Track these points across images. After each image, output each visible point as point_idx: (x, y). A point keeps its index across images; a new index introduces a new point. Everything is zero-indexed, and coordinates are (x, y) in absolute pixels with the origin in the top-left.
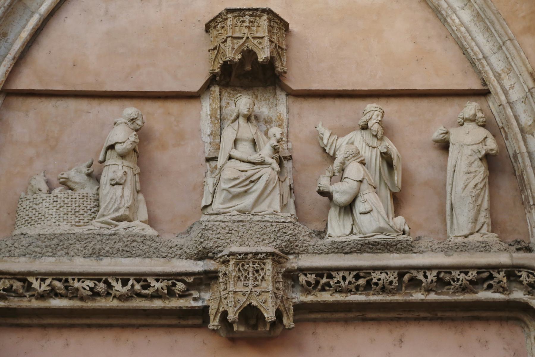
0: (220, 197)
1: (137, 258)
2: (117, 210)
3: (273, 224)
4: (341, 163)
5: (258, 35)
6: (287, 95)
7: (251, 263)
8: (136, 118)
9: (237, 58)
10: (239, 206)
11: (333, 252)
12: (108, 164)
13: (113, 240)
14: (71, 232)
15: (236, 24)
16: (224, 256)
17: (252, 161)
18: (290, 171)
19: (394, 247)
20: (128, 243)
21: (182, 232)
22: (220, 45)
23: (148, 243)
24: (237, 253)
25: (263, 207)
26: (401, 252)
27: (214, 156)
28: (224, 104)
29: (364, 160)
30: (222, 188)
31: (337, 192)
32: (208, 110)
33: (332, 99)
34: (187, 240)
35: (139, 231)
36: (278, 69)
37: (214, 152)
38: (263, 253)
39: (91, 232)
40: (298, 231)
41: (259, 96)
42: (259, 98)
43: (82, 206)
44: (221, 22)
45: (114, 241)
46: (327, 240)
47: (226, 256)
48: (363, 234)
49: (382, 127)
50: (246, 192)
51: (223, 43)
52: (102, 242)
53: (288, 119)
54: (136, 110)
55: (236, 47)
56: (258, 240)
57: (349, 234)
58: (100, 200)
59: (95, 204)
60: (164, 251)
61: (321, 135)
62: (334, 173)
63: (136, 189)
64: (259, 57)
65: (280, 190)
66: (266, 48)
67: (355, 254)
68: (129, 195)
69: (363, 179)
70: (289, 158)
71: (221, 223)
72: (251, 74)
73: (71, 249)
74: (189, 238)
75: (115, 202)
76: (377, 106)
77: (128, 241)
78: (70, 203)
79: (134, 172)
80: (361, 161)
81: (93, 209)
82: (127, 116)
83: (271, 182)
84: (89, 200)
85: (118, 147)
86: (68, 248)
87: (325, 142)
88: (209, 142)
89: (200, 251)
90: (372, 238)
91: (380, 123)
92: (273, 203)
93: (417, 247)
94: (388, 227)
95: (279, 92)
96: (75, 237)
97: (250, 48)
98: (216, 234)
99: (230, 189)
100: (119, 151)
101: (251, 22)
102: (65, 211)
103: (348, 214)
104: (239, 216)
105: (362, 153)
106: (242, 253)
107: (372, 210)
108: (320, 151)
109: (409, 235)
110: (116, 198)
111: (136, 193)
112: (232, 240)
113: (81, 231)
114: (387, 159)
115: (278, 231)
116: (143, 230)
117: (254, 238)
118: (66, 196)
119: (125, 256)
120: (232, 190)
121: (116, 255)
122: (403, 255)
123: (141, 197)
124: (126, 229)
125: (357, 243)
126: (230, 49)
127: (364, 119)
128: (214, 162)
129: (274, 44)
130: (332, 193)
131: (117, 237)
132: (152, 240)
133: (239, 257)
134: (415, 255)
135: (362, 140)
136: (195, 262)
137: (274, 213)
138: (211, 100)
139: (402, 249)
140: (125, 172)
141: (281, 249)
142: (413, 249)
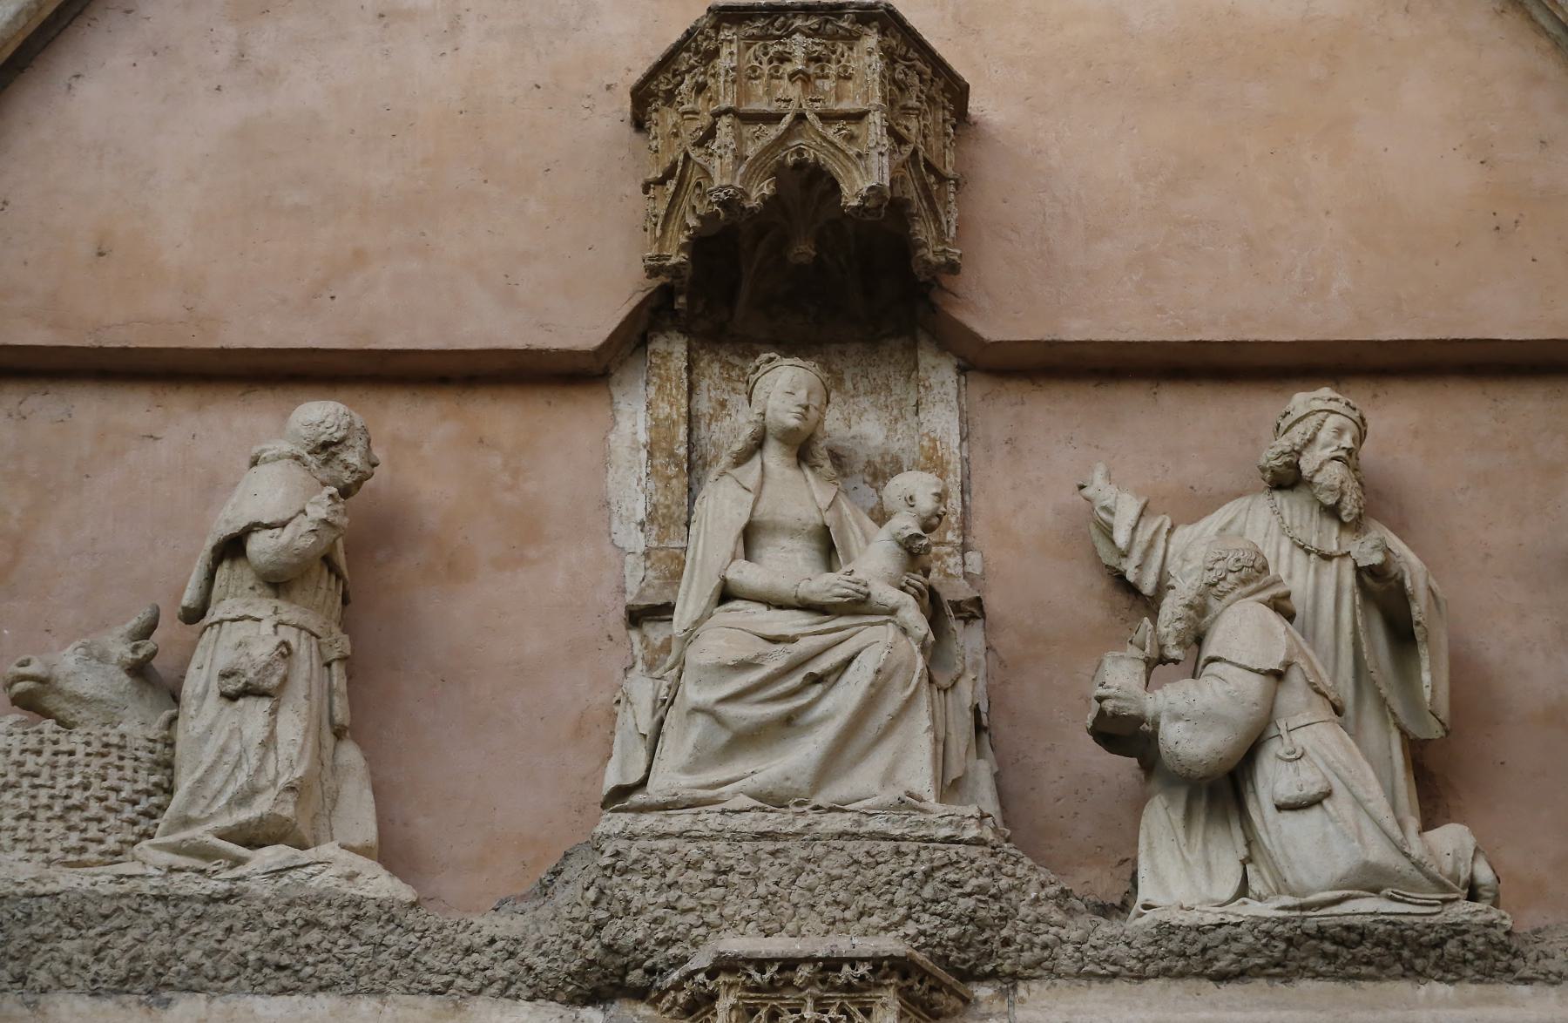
0: (675, 750)
1: (320, 996)
2: (244, 798)
3: (904, 846)
4: (1190, 606)
5: (846, 106)
6: (962, 370)
7: (810, 1003)
8: (341, 441)
9: (754, 194)
10: (758, 778)
11: (1165, 973)
12: (215, 619)
13: (218, 919)
14: (40, 889)
15: (754, 69)
16: (691, 975)
17: (817, 598)
18: (976, 665)
19: (1434, 954)
20: (285, 932)
21: (521, 891)
22: (687, 157)
23: (373, 930)
24: (748, 961)
25: (863, 782)
26: (1461, 978)
27: (659, 602)
28: (704, 405)
29: (1287, 596)
30: (689, 705)
31: (1178, 717)
32: (641, 426)
33: (1145, 385)
34: (536, 921)
35: (333, 882)
36: (921, 252)
37: (664, 586)
38: (863, 960)
39: (128, 886)
40: (1011, 881)
41: (847, 376)
42: (849, 385)
43: (96, 783)
44: (688, 71)
45: (226, 923)
46: (1138, 923)
47: (701, 977)
48: (1292, 894)
49: (1358, 480)
50: (788, 722)
51: (700, 143)
52: (172, 927)
53: (965, 461)
54: (342, 408)
55: (751, 150)
56: (838, 914)
57: (1234, 899)
58: (177, 763)
59: (154, 779)
60: (437, 964)
61: (1104, 515)
62: (1162, 647)
63: (331, 719)
64: (846, 190)
65: (933, 717)
66: (874, 153)
67: (1262, 982)
68: (300, 740)
69: (1288, 665)
70: (973, 610)
71: (680, 843)
72: (813, 269)
73: (36, 961)
74: (546, 912)
75: (237, 765)
76: (1335, 395)
77: (283, 924)
78: (46, 772)
79: (325, 650)
80: (1274, 597)
81: (143, 798)
82: (304, 432)
83: (898, 682)
84: (128, 763)
85: (259, 545)
86: (24, 954)
87: (1121, 538)
88: (641, 548)
89: (592, 962)
90: (1336, 910)
91: (1349, 458)
92: (910, 762)
93: (1532, 956)
94: (1404, 865)
95: (926, 359)
96: (58, 907)
97: (810, 156)
98: (659, 889)
99: (721, 709)
100: (263, 558)
101: (811, 59)
102: (24, 803)
103: (1226, 821)
104: (759, 814)
105: (1279, 569)
106: (771, 961)
107: (1328, 794)
108: (1102, 584)
109: (1496, 904)
110: (238, 751)
111: (329, 740)
112: (728, 911)
113: (86, 884)
114: (1383, 593)
115: (928, 875)
116: (351, 877)
117: (821, 907)
118: (32, 742)
119: (270, 987)
120: (731, 711)
121: (230, 984)
122: (1474, 989)
123: (350, 754)
124: (278, 873)
125: (1267, 933)
126: (729, 157)
127: (1284, 443)
128: (661, 626)
129: (907, 150)
130: (1156, 724)
131: (237, 907)
132: (389, 921)
133: (757, 977)
134: (1524, 990)
135: (1275, 529)
136: (569, 1013)
137: (908, 804)
138: (652, 390)
139: (1465, 961)
140: (285, 644)
141: (939, 951)
142: (1515, 963)
